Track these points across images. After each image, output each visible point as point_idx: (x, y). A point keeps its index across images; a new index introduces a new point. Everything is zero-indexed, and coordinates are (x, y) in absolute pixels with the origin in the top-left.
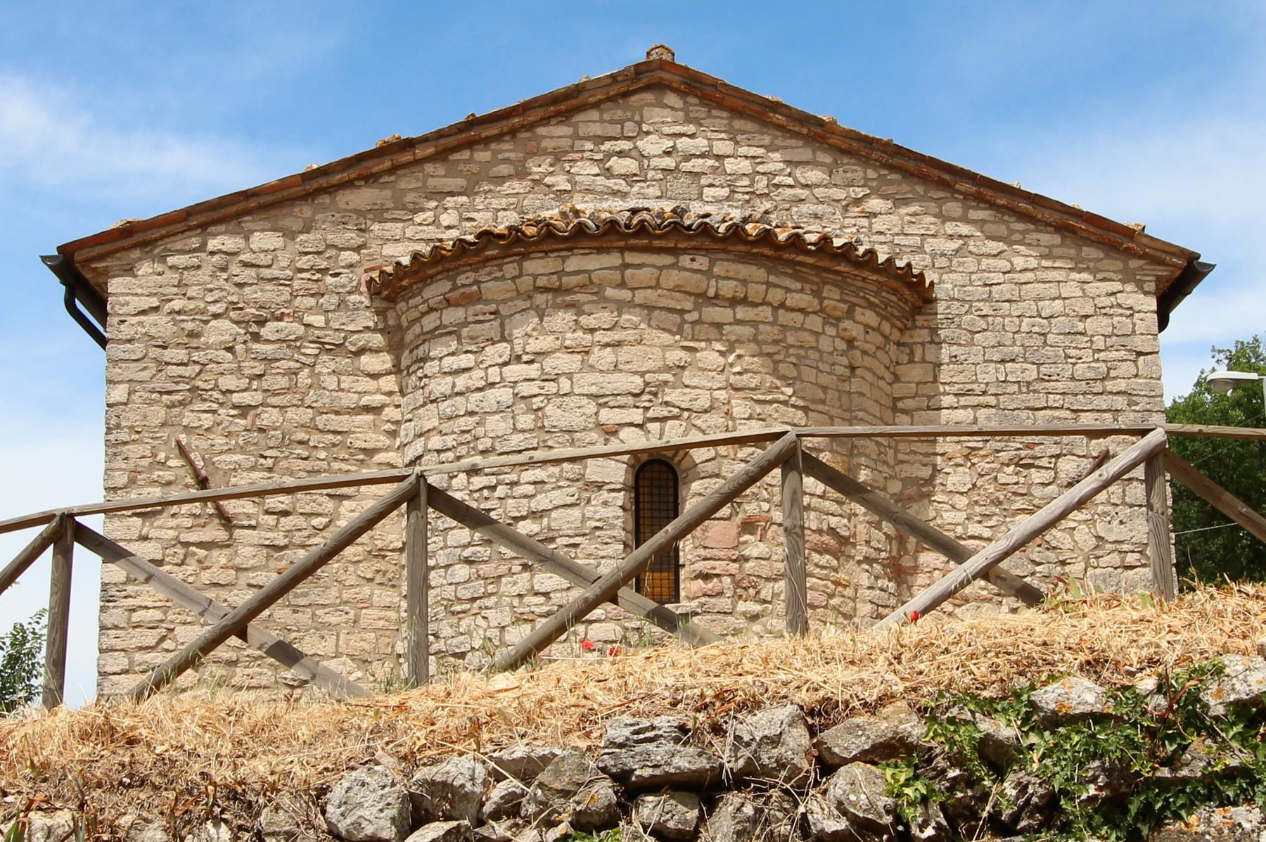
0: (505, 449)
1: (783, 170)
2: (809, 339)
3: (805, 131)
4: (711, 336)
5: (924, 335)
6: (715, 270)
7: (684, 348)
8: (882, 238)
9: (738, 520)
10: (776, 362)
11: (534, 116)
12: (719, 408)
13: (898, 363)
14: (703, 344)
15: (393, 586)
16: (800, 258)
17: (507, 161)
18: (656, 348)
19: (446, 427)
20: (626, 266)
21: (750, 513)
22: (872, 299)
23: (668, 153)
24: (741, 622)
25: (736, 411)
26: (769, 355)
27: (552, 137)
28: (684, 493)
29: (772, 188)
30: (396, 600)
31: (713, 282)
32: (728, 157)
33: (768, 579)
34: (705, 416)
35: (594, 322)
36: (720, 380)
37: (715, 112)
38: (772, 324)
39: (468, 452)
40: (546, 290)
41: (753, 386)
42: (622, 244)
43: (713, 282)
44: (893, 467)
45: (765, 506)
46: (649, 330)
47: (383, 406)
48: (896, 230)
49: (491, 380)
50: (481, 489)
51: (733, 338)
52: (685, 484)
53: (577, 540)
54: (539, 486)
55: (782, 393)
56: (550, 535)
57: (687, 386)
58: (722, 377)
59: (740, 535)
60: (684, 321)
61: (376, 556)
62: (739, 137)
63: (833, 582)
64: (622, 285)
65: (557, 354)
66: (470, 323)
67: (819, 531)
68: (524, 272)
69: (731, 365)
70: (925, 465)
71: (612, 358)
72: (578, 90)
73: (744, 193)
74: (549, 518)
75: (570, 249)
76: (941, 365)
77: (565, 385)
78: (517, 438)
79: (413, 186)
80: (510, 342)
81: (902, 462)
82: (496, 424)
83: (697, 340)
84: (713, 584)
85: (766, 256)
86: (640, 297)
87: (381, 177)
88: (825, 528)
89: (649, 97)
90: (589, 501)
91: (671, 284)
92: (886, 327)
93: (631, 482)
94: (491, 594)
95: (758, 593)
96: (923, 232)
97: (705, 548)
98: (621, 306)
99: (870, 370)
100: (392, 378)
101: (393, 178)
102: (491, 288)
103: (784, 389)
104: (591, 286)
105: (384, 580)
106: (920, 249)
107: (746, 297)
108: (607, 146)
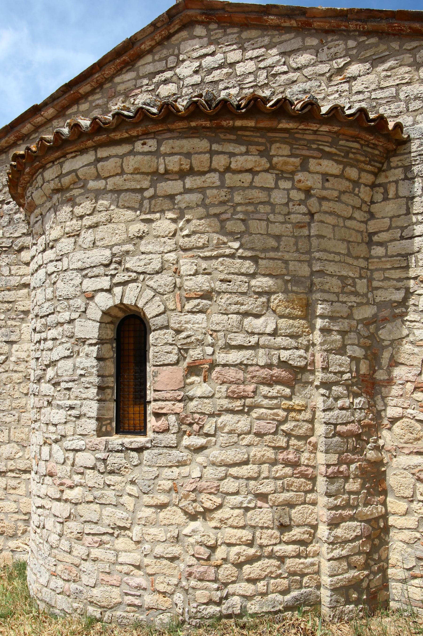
1: (279, 61)
2: (262, 196)
3: (294, 23)
4: (165, 207)
5: (399, 173)
6: (162, 149)
7: (143, 221)
8: (361, 97)
9: (184, 364)
10: (223, 222)
11: (108, 71)
13: (372, 202)
14: (158, 215)
17: (98, 106)
18: (124, 223)
21: (195, 357)
22: (327, 149)
23: (196, 72)
24: (185, 455)
26: (216, 215)
29: (270, 78)
32: (238, 62)
33: (212, 415)
34: (156, 277)
36: (171, 244)
37: (229, 31)
38: (222, 186)
41: (201, 244)
42: (90, 143)
45: (209, 350)
46: (117, 210)
48: (373, 87)
51: (183, 206)
53: (70, 385)
55: (229, 247)
57: (143, 253)
58: (173, 241)
59: (186, 377)
60: (143, 198)
63: (284, 410)
64: (98, 177)
67: (270, 366)
70: (398, 289)
72: (130, 44)
73: (249, 88)
75: (64, 156)
76: (414, 197)
81: (377, 288)
85: (204, 127)
86: (111, 183)
87: (31, 135)
88: (275, 362)
89: (184, 34)
92: (353, 173)
95: (201, 428)
96: (398, 82)
98: (98, 194)
103: (230, 244)
104: (79, 182)
106: (396, 98)
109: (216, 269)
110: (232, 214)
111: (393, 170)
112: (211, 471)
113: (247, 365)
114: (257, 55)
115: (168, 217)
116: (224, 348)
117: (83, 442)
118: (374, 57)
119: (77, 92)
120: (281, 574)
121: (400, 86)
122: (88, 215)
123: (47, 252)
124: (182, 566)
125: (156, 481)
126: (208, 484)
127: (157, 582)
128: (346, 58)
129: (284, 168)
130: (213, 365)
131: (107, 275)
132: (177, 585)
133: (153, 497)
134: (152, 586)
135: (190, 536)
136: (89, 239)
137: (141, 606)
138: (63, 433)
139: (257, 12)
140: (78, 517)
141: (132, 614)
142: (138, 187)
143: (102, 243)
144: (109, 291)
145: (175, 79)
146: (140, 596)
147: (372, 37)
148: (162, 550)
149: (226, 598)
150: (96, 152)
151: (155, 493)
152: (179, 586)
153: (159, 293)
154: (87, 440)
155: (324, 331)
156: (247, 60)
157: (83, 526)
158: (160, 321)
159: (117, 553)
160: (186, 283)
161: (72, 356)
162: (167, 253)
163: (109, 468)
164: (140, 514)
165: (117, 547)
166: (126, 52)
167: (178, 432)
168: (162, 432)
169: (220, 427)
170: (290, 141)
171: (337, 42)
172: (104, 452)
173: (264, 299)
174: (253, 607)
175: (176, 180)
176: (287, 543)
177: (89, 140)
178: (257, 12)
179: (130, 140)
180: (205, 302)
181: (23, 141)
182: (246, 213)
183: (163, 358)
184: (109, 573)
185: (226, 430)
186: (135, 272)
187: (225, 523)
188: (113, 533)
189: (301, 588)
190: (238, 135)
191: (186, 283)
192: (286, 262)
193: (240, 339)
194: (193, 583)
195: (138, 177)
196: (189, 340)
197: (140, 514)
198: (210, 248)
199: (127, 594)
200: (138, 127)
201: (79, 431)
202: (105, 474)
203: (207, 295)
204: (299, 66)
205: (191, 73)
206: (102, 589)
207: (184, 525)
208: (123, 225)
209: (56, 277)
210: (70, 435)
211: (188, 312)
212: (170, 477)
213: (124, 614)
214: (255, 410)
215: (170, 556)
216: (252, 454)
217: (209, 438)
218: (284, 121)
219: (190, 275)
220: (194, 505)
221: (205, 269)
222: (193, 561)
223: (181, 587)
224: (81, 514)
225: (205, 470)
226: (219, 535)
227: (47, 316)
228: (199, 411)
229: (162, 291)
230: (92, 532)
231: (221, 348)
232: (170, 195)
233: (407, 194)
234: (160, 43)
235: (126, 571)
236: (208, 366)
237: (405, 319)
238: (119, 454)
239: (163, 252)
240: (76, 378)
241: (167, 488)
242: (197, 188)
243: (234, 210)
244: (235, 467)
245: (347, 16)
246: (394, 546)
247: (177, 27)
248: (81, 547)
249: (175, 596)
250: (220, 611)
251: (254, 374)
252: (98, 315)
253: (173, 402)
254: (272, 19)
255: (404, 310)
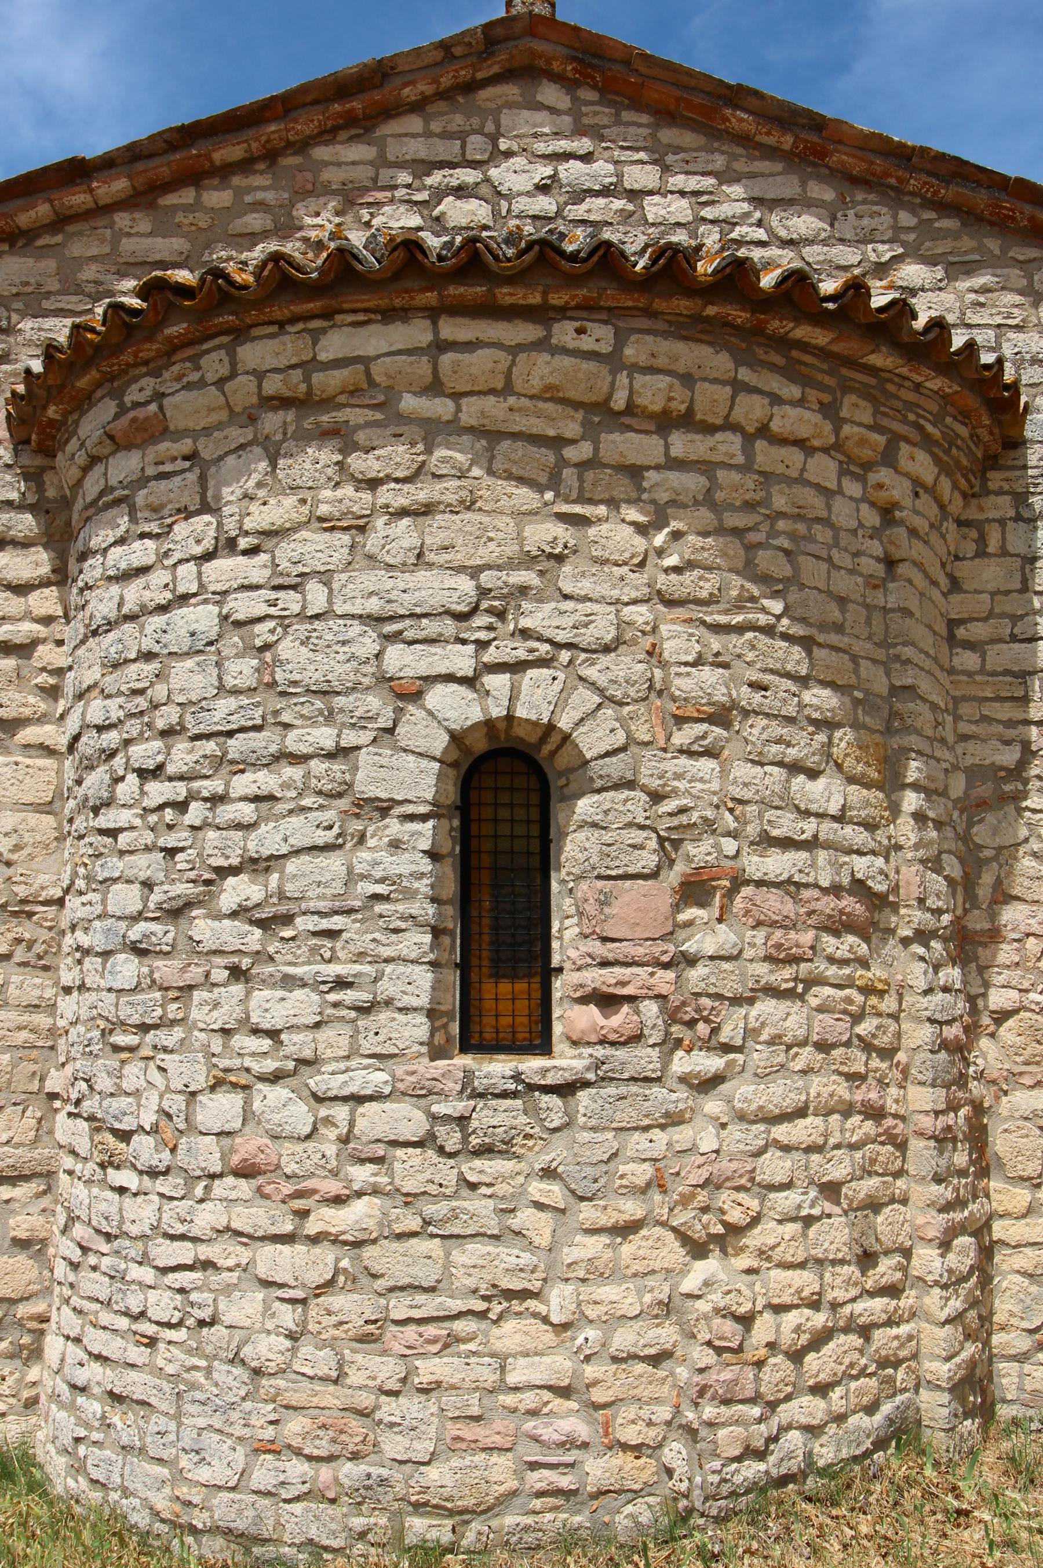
0: (202, 729)
1: (747, 215)
2: (816, 503)
4: (618, 493)
5: (1001, 506)
6: (629, 351)
7: (562, 517)
9: (673, 877)
11: (304, 125)
12: (634, 642)
13: (957, 558)
14: (602, 510)
15: (46, 968)
16: (802, 332)
17: (259, 206)
18: (506, 519)
19: (110, 682)
20: (441, 346)
22: (929, 428)
23: (543, 188)
25: (670, 649)
27: (339, 164)
28: (561, 817)
30: (49, 993)
31: (623, 379)
32: (651, 193)
33: (736, 1001)
34: (605, 660)
35: (377, 466)
36: (637, 583)
37: (627, 116)
38: (746, 468)
39: (142, 733)
40: (283, 402)
41: (704, 594)
42: (431, 298)
43: (623, 379)
44: (951, 749)
45: (730, 846)
46: (489, 481)
47: (35, 643)
49: (181, 589)
50: (161, 807)
51: (664, 497)
52: (564, 798)
53: (336, 922)
54: (264, 806)
55: (764, 610)
56: (283, 909)
57: (566, 597)
58: (640, 578)
59: (677, 908)
61: (15, 914)
62: (670, 159)
64: (434, 387)
65: (304, 534)
66: (149, 479)
67: (835, 890)
68: (240, 368)
69: (660, 552)
70: (1007, 743)
71: (412, 540)
72: (378, 74)
74: (282, 873)
75: (327, 315)
77: (317, 596)
78: (225, 705)
79: (94, 251)
80: (215, 511)
81: (964, 738)
82: (189, 678)
83: (591, 501)
84: (621, 1019)
86: (471, 411)
87: (38, 236)
88: (846, 881)
89: (510, 91)
90: (362, 839)
91: (536, 384)
92: (945, 485)
93: (452, 795)
94: (173, 1023)
95: (715, 1031)
97: (605, 939)
98: (432, 432)
99: (919, 566)
100: (52, 592)
101: (59, 238)
102: (187, 407)
103: (766, 602)
105: (30, 957)
107: (690, 412)
108: (436, 178)
109: (739, 656)
110: (769, 536)
111: (992, 497)
112: (738, 1135)
113: (798, 885)
114: (697, 187)
115: (628, 518)
116: (757, 844)
117: (383, 1076)
118: (951, 259)
119: (208, 157)
120: (866, 1366)
121: (1004, 330)
122: (397, 480)
123: (215, 563)
124: (682, 1372)
125: (612, 1164)
126: (734, 1165)
127: (620, 1421)
128: (895, 246)
129: (856, 451)
130: (738, 881)
131: (464, 642)
132: (668, 1423)
133: (605, 1208)
134: (606, 1434)
135: (699, 1297)
136: (406, 543)
137: (574, 1493)
138: (307, 1053)
139: (708, 93)
140: (364, 1280)
141: (549, 1516)
142: (551, 433)
143: (448, 557)
144: (469, 682)
145: (485, 190)
146: (572, 1465)
147: (948, 217)
148: (631, 1338)
149: (775, 1439)
150: (435, 324)
151: (611, 1195)
152: (675, 1425)
153: (611, 699)
154: (400, 1071)
155: (919, 817)
156: (672, 192)
157: (383, 1301)
158: (615, 767)
159: (502, 1361)
160: (677, 682)
161: (340, 846)
162: (627, 604)
163: (474, 1141)
164: (569, 1254)
165: (498, 1346)
166: (361, 91)
167: (664, 1042)
168: (624, 1044)
169: (754, 1030)
170: (878, 394)
171: (875, 208)
172: (461, 1100)
173: (822, 737)
174: (825, 1453)
175: (647, 432)
176: (872, 1294)
177: (432, 290)
178: (708, 93)
179: (542, 314)
180: (717, 731)
181: (12, 245)
182: (792, 536)
183: (625, 859)
184: (477, 1419)
185: (764, 1037)
186: (549, 641)
187: (769, 1259)
188: (488, 1310)
189: (894, 1395)
190: (788, 358)
191: (677, 682)
192: (854, 659)
193: (786, 825)
194: (709, 1411)
195: (550, 406)
196: (684, 819)
197: (569, 1254)
198: (722, 606)
199: (534, 1466)
200: (579, 287)
201: (368, 1045)
202: (461, 1158)
203: (721, 716)
204: (795, 236)
205: (530, 187)
206: (456, 1462)
207: (681, 1271)
208: (508, 520)
209: (272, 631)
210: (337, 1059)
211: (681, 751)
212: (648, 1155)
213: (529, 1520)
214: (815, 990)
215: (652, 1351)
216: (813, 1093)
217: (732, 1056)
218: (884, 349)
219: (686, 664)
220: (705, 1218)
221: (718, 654)
222: (708, 1357)
223: (680, 1426)
224: (376, 1268)
225: (724, 1133)
226: (757, 1288)
227: (230, 734)
228: (712, 990)
229: (619, 694)
230: (417, 1314)
231: (752, 843)
232: (633, 466)
233: (1022, 550)
234: (444, 95)
235: (532, 1406)
236: (727, 883)
237: (1024, 804)
238: (508, 1103)
239: (618, 601)
240: (357, 903)
241: (641, 1182)
242: (697, 462)
243: (772, 526)
244: (781, 1123)
245: (909, 159)
246: (1005, 1284)
247: (496, 69)
248: (378, 1359)
249: (666, 1450)
250: (767, 1472)
251: (814, 905)
252: (440, 742)
253: (650, 969)
254: (741, 120)
255: (1020, 787)
